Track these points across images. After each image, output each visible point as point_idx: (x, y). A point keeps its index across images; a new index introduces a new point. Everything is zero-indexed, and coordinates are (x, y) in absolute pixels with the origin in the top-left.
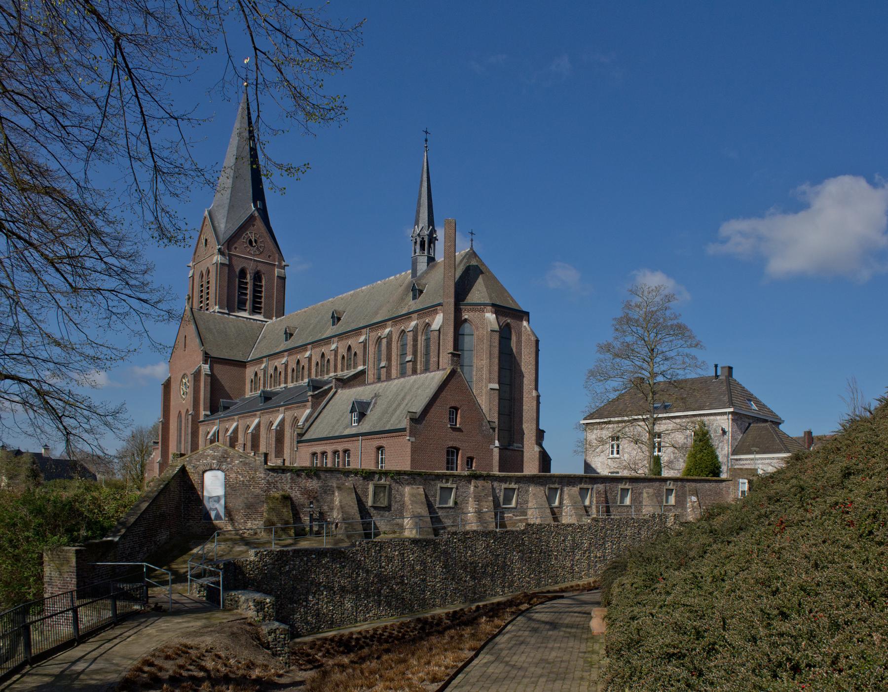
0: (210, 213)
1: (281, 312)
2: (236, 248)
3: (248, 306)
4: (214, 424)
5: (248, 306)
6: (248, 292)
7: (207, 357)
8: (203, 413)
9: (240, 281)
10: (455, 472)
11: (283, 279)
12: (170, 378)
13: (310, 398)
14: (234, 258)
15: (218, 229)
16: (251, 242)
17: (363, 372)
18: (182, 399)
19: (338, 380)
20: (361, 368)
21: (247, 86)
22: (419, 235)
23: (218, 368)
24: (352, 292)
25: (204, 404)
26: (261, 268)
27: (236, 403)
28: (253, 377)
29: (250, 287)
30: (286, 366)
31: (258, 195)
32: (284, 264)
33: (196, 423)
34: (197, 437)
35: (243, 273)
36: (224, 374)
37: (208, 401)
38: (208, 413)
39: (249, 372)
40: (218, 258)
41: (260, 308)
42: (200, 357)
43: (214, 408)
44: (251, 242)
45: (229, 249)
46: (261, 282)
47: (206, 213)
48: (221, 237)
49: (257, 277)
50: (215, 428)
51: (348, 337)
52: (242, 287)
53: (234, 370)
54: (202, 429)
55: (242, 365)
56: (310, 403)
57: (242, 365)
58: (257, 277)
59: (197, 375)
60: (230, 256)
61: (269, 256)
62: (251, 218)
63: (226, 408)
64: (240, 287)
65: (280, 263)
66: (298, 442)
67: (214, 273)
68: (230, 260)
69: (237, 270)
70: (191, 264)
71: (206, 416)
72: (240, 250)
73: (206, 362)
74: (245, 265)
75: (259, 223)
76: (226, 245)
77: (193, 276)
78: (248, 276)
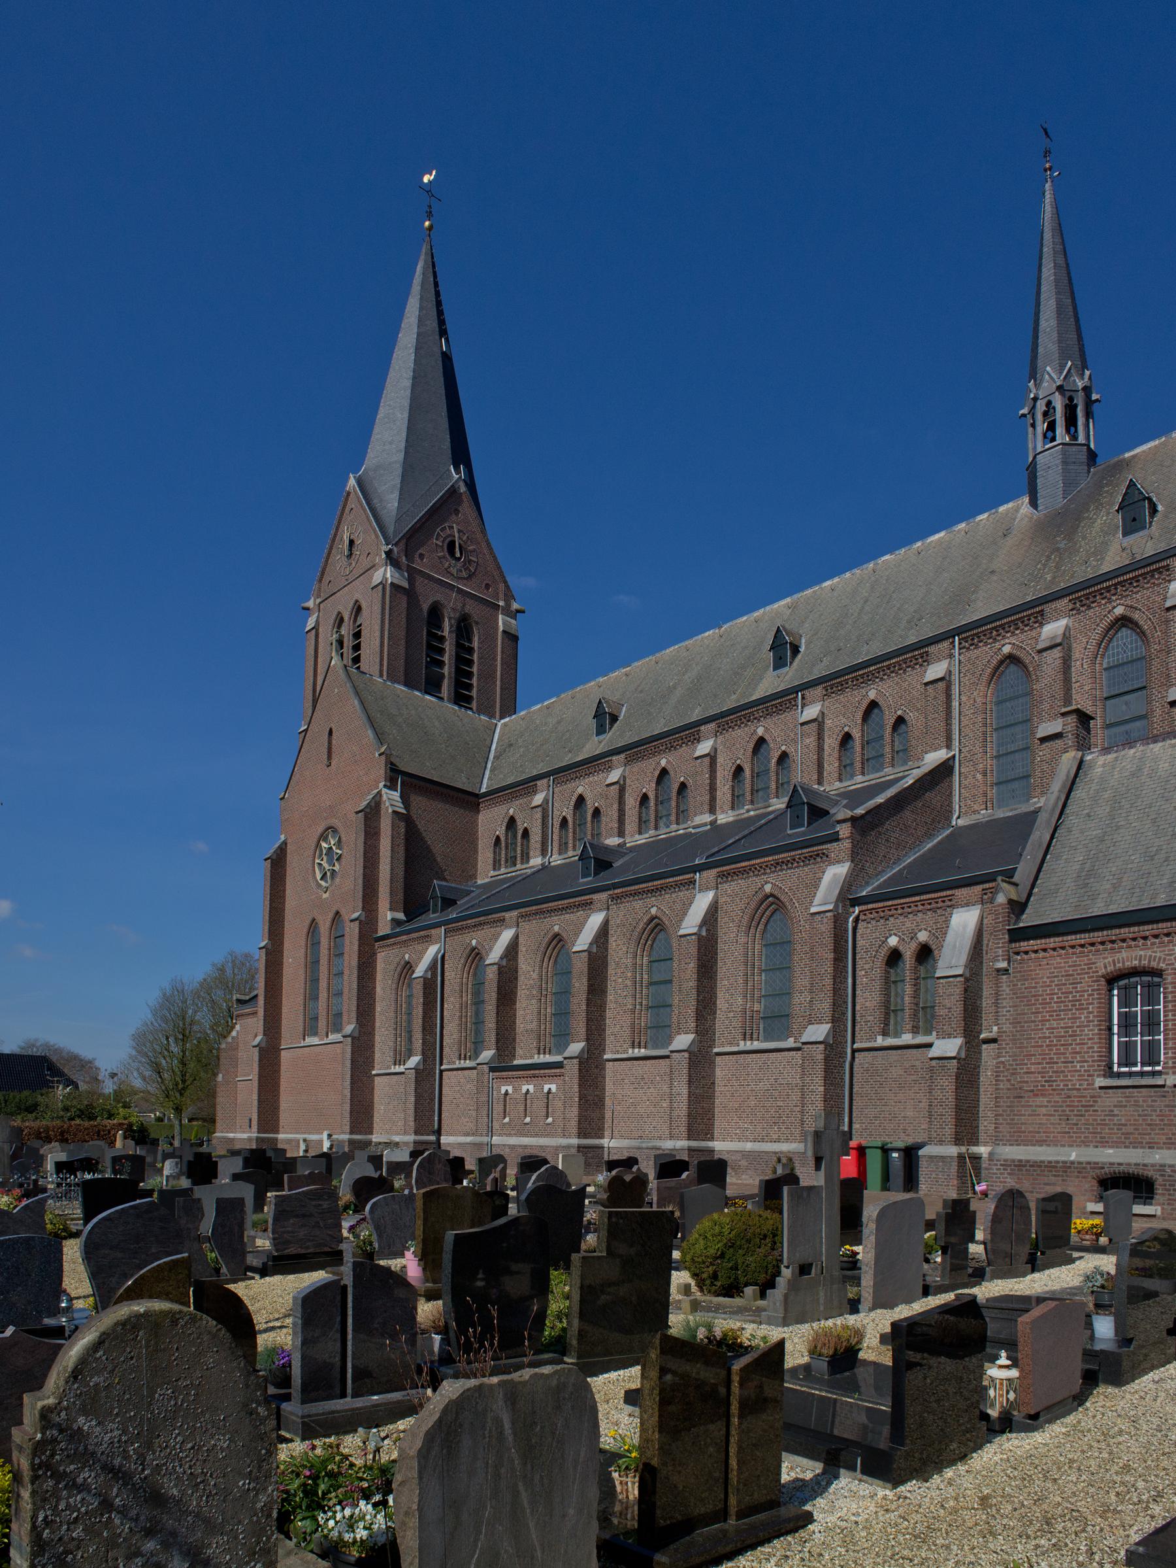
0: (360, 482)
1: (509, 708)
2: (421, 556)
3: (446, 688)
4: (428, 940)
5: (446, 688)
6: (446, 658)
7: (394, 775)
8: (387, 916)
9: (430, 634)
10: (1134, 1069)
11: (512, 638)
12: (285, 843)
13: (844, 830)
14: (419, 580)
15: (383, 513)
16: (451, 546)
17: (944, 770)
18: (326, 889)
19: (239, 1001)
20: (940, 755)
21: (431, 228)
22: (1060, 388)
23: (417, 800)
24: (788, 600)
25: (392, 893)
26: (471, 608)
27: (469, 893)
28: (501, 831)
29: (449, 647)
30: (622, 787)
31: (460, 454)
32: (515, 606)
33: (369, 941)
34: (372, 977)
35: (435, 614)
36: (434, 818)
37: (400, 884)
38: (401, 916)
39: (490, 822)
40: (385, 574)
41: (469, 699)
42: (380, 770)
43: (414, 904)
44: (451, 546)
45: (408, 553)
46: (470, 640)
47: (352, 482)
48: (391, 530)
49: (464, 628)
50: (432, 951)
51: (868, 679)
52: (434, 647)
53: (454, 814)
54: (385, 961)
55: (470, 801)
56: (847, 844)
57: (470, 801)
58: (464, 628)
59: (372, 813)
60: (412, 574)
61: (487, 586)
62: (453, 492)
63: (449, 903)
64: (430, 647)
65: (508, 605)
66: (1017, 935)
67: (377, 608)
68: (411, 580)
69: (425, 607)
70: (310, 604)
71: (396, 922)
72: (430, 560)
73: (392, 786)
74: (438, 597)
75: (466, 507)
76: (402, 545)
77: (316, 628)
78: (446, 624)
